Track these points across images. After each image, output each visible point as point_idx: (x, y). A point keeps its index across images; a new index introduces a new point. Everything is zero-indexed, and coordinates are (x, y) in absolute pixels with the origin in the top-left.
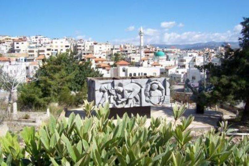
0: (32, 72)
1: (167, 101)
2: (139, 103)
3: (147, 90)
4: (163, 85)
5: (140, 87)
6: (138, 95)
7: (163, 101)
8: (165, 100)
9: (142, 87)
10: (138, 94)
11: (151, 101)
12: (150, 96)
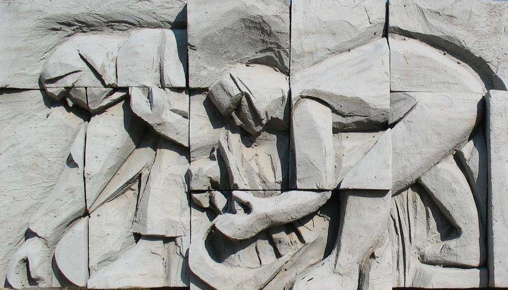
6: (450, 167)
10: (460, 160)
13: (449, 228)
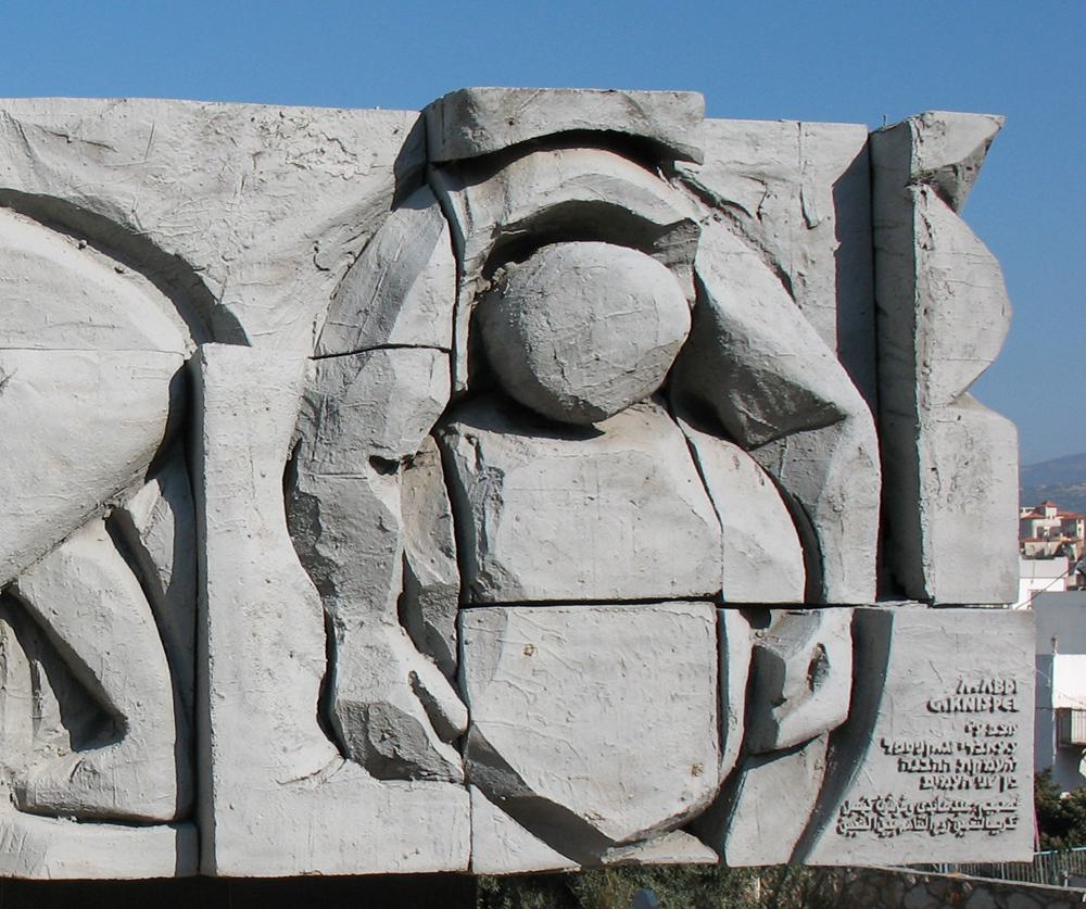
0: (813, 788)
1: (946, 732)
2: (144, 769)
3: (376, 413)
4: (846, 355)
5: (166, 335)
6: (96, 551)
7: (847, 741)
8: (896, 724)
9: (209, 320)
10: (122, 532)
11: (495, 724)
12: (456, 598)
13: (93, 719)
